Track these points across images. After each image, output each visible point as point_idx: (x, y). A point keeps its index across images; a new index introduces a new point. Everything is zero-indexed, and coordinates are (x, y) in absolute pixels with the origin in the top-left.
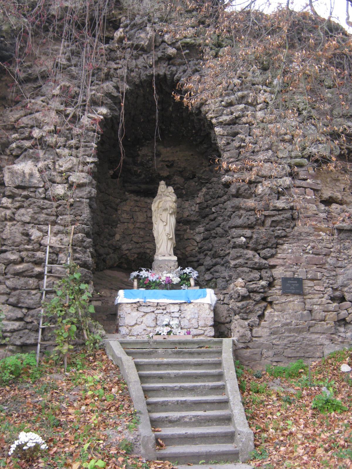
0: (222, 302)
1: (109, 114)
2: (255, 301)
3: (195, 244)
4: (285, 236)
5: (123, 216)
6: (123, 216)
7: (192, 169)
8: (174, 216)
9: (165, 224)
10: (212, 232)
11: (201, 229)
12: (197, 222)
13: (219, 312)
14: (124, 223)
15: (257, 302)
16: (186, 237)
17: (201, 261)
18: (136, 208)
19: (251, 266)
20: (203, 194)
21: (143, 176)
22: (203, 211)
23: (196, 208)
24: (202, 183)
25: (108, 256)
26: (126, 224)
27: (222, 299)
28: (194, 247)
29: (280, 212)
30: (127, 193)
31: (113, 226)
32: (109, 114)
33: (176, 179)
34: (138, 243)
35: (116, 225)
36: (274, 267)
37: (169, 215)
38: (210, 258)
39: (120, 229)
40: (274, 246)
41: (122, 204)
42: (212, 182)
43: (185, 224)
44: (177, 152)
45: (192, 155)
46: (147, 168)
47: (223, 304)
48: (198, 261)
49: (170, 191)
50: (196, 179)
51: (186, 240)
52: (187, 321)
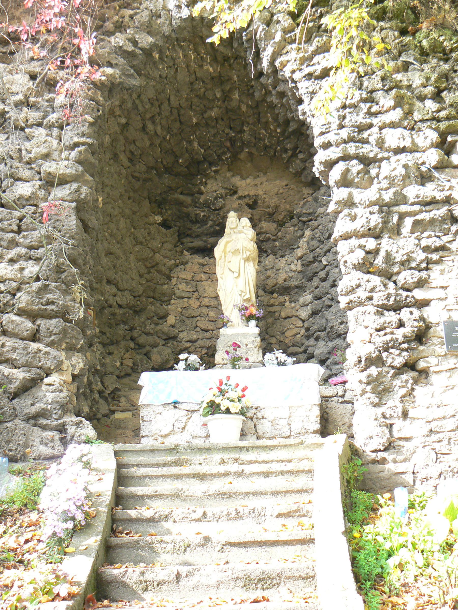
0: (341, 400)
1: (117, 76)
2: (393, 367)
3: (300, 323)
4: (443, 248)
5: (180, 286)
6: (180, 286)
7: (288, 206)
8: (251, 263)
9: (236, 275)
10: (324, 299)
11: (307, 297)
12: (301, 288)
13: (335, 417)
14: (183, 298)
15: (399, 371)
16: (283, 315)
17: (310, 350)
18: (202, 275)
19: (380, 303)
20: (305, 239)
21: (210, 223)
22: (309, 268)
23: (298, 266)
24: (304, 222)
25: (155, 349)
26: (186, 300)
27: (340, 393)
28: (297, 330)
29: (428, 208)
30: (185, 252)
31: (164, 302)
32: (117, 76)
33: (264, 226)
34: (207, 331)
35: (169, 301)
36: (425, 303)
37: (243, 262)
38: (324, 343)
39: (176, 306)
40: (424, 265)
41: (178, 269)
42: (318, 216)
43: (281, 294)
44: (262, 183)
45: (287, 185)
46: (216, 210)
47: (341, 403)
48: (305, 351)
49: (244, 224)
50: (295, 221)
51: (285, 318)
52: (270, 424)
